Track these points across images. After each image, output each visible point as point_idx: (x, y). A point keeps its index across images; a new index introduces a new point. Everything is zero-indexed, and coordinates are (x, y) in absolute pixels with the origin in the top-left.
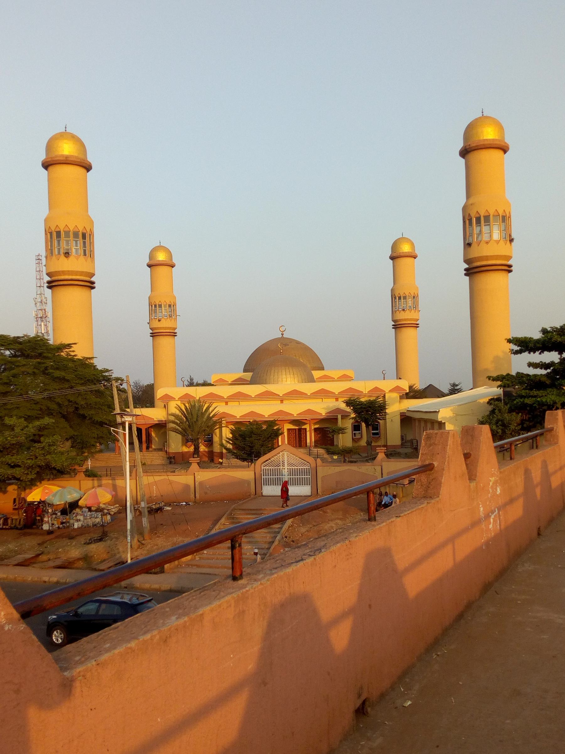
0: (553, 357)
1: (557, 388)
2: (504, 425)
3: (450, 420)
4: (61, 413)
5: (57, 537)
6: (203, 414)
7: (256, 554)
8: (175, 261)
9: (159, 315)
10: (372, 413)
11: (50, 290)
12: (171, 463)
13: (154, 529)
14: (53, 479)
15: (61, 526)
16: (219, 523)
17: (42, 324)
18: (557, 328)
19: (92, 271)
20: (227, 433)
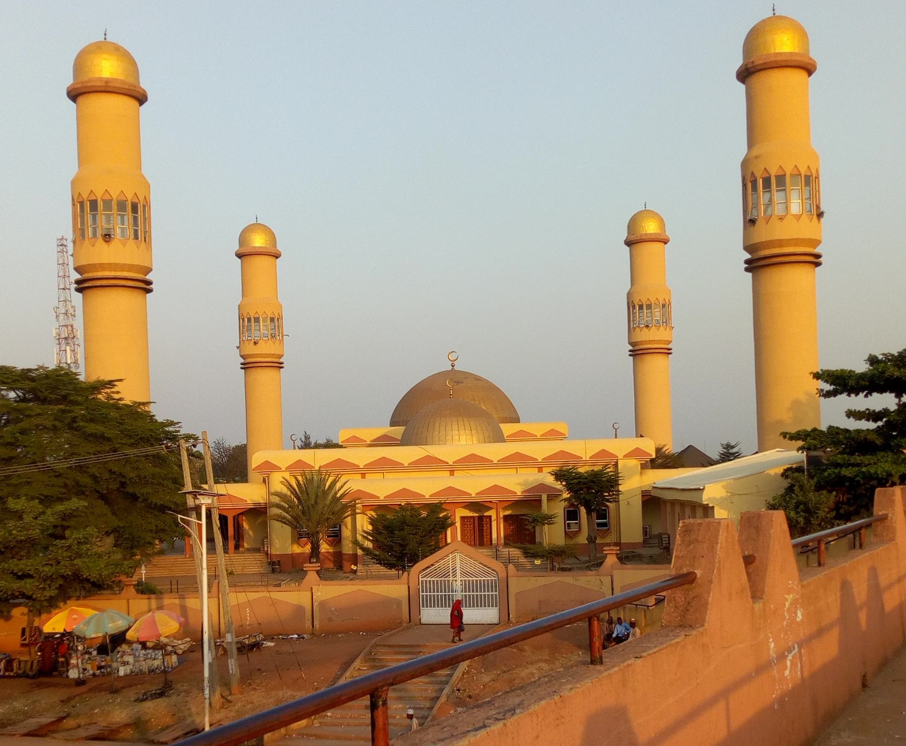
0: (886, 401)
1: (892, 451)
2: (807, 511)
3: (722, 502)
4: (98, 492)
5: (91, 690)
6: (325, 493)
7: (410, 717)
8: (280, 247)
9: (255, 335)
10: (597, 492)
11: (80, 295)
12: (273, 571)
13: (247, 678)
14: (85, 597)
15: (98, 672)
16: (352, 667)
17: (68, 348)
18: (893, 355)
19: (147, 264)
20: (363, 523)
